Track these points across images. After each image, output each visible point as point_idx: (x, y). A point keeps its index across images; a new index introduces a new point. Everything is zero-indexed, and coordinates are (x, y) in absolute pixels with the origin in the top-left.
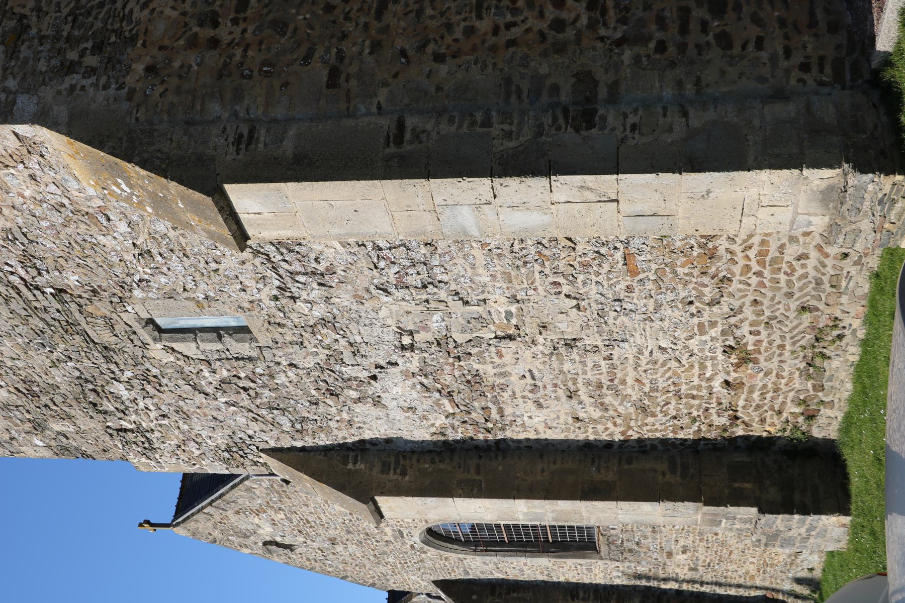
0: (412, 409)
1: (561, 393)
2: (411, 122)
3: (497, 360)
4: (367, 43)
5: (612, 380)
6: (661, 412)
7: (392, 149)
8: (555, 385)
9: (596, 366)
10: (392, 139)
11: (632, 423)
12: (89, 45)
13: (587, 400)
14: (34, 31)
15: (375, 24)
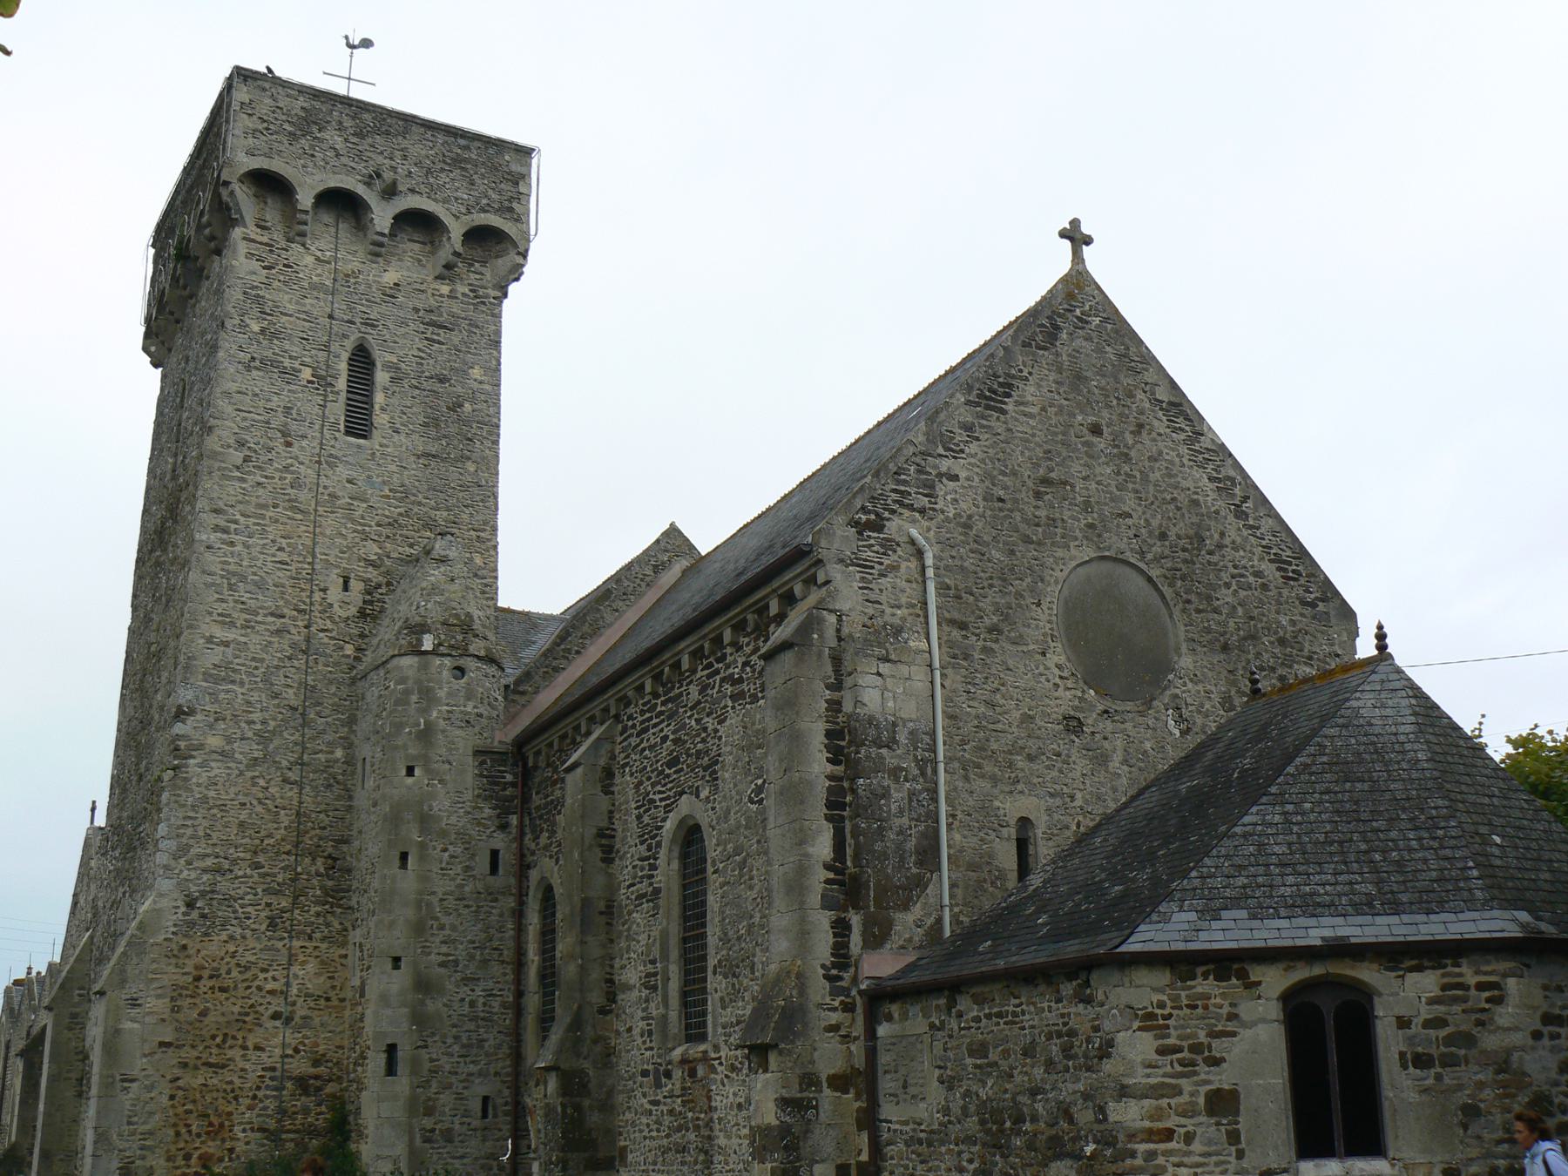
2: (135, 1085)
15: (199, 1063)
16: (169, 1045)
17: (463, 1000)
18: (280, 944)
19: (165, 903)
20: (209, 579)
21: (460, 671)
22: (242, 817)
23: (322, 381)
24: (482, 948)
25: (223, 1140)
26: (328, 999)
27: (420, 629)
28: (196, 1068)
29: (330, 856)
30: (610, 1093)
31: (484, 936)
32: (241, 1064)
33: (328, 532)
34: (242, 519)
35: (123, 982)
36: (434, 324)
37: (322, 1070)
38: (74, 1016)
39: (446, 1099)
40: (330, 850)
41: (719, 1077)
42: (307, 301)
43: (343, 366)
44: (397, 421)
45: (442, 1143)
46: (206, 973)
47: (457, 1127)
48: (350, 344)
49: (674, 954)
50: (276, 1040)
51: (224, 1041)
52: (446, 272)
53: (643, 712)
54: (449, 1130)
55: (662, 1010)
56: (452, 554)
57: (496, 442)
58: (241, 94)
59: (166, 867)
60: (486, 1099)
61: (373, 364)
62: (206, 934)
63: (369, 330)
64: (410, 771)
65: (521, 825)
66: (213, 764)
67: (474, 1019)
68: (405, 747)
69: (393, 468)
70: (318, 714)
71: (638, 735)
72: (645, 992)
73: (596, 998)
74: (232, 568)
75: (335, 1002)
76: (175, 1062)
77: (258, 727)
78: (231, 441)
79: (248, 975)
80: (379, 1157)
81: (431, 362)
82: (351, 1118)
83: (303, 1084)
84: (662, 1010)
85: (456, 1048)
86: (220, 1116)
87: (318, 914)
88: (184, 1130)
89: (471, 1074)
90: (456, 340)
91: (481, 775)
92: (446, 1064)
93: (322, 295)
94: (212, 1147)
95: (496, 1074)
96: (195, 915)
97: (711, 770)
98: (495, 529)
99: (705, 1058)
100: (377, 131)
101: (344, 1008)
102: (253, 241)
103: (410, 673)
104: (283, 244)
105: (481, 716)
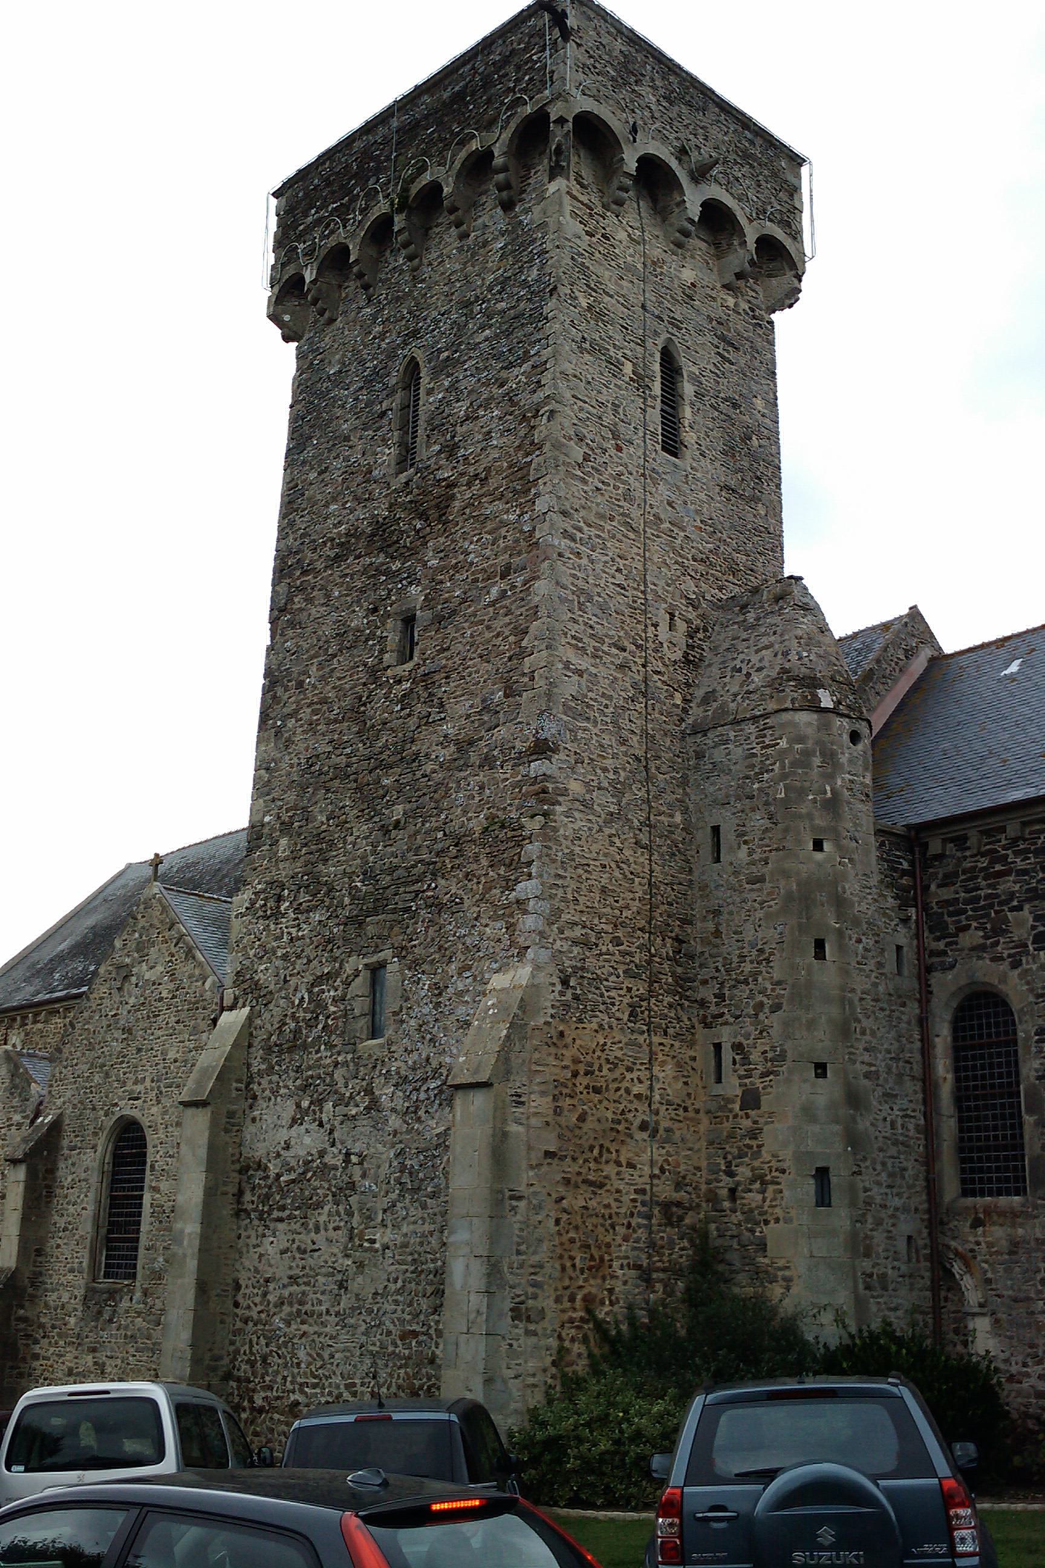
0: (287, 1147)
1: (297, 1272)
2: (522, 1204)
3: (331, 1226)
4: (569, 1176)
5: (306, 1313)
6: (271, 1351)
8: (304, 1268)
9: (320, 1302)
11: (260, 1327)
12: (579, 992)
13: (286, 1293)
14: (587, 953)
15: (580, 1179)
18: (641, 1039)
19: (542, 978)
20: (562, 592)
23: (640, 381)
24: (896, 1059)
25: (604, 1278)
31: (896, 1045)
34: (586, 528)
35: (508, 1072)
38: (231, 1115)
39: (879, 1237)
42: (624, 283)
43: (657, 367)
45: (879, 1292)
46: (582, 1068)
47: (890, 1272)
48: (660, 342)
50: (646, 1153)
51: (601, 1154)
57: (778, 486)
60: (910, 1238)
62: (580, 1021)
64: (818, 846)
66: (577, 815)
67: (896, 1143)
69: (702, 496)
70: (658, 768)
74: (580, 583)
76: (558, 1177)
79: (617, 1074)
86: (600, 1248)
87: (670, 1006)
91: (882, 858)
92: (876, 1192)
93: (636, 281)
94: (593, 1287)
103: (810, 731)
104: (599, 209)
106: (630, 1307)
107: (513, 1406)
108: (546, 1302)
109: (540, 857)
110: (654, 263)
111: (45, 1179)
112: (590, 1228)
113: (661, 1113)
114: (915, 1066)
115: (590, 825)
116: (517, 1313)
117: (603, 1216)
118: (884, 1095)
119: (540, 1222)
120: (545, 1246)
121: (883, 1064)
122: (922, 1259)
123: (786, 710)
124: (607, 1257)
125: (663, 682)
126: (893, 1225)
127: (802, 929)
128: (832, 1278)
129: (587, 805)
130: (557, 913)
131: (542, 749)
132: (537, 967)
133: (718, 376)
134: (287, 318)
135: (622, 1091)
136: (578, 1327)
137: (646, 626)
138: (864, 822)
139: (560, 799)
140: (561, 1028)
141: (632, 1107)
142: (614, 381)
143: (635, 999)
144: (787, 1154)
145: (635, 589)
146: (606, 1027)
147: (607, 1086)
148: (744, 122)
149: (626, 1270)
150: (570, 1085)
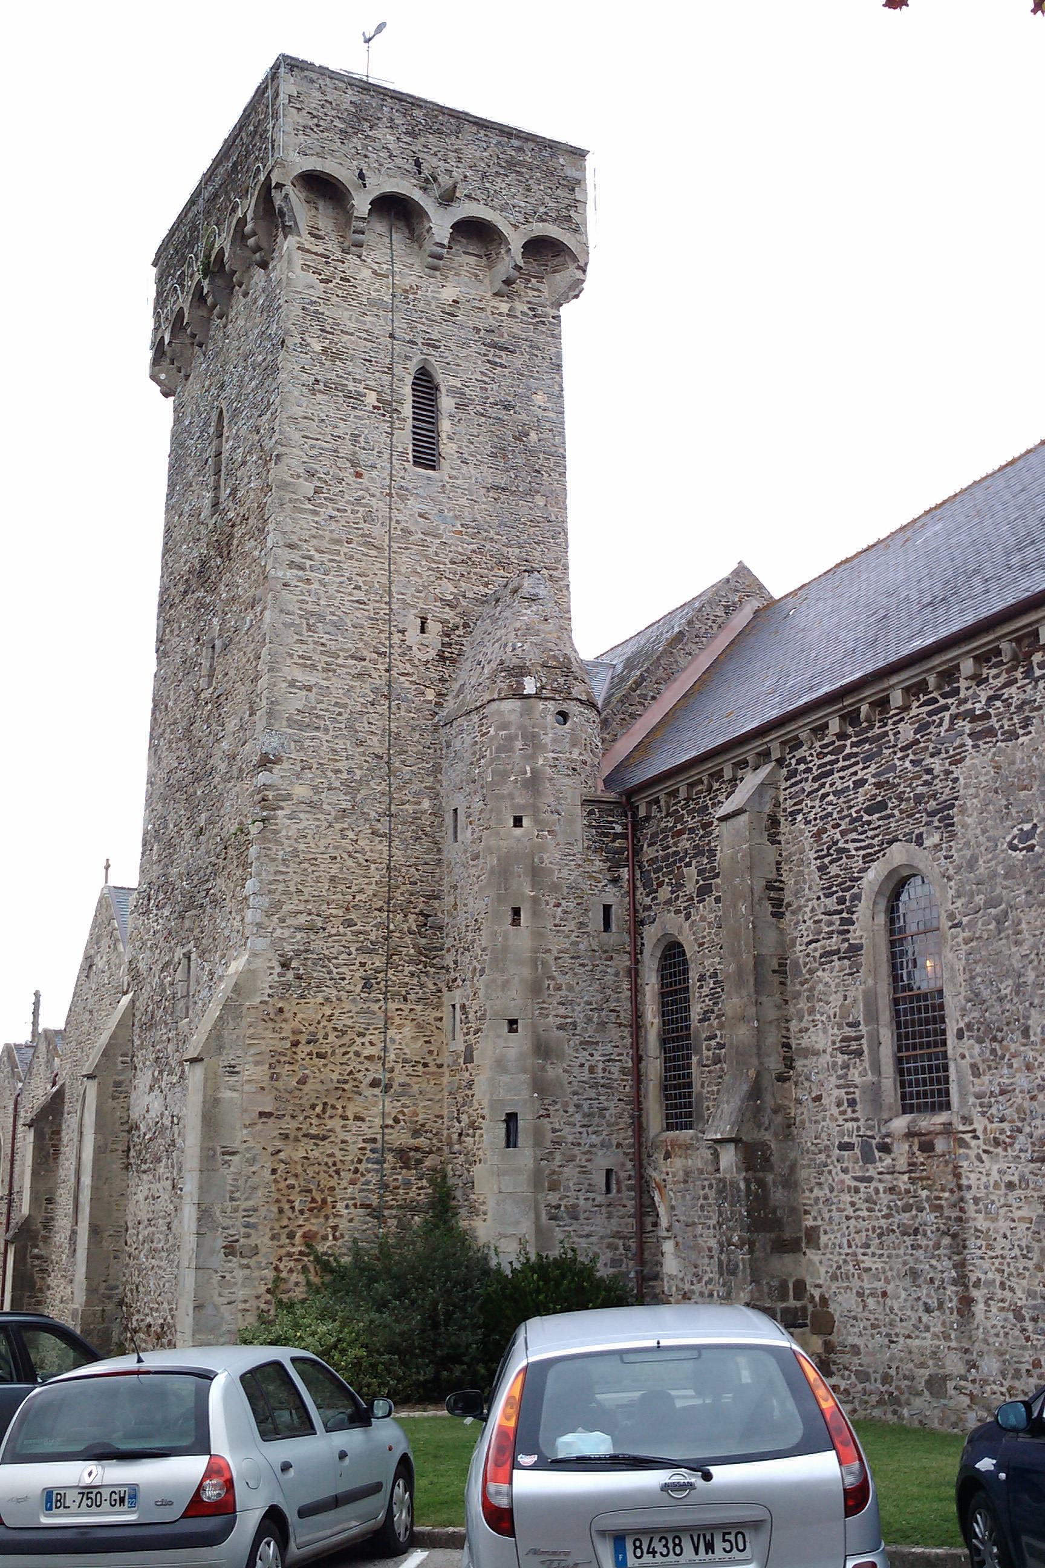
7: (219, 1150)
10: (884, 813)
14: (313, 937)
15: (300, 1134)
16: (269, 1115)
17: (582, 1065)
18: (375, 1007)
19: (260, 963)
20: (288, 619)
21: (564, 716)
22: (333, 872)
23: (387, 407)
25: (327, 1217)
26: (425, 1065)
27: (520, 672)
28: (297, 1140)
29: (421, 913)
30: (793, 1168)
32: (342, 1135)
33: (403, 570)
34: (317, 555)
35: (221, 1048)
36: (497, 346)
37: (421, 1141)
38: (118, 1084)
40: (421, 906)
41: (972, 1153)
42: (367, 319)
43: (408, 390)
44: (465, 450)
45: (568, 1221)
46: (303, 1039)
47: (582, 1202)
48: (413, 366)
49: (885, 1015)
50: (376, 1109)
51: (324, 1111)
52: (505, 288)
53: (821, 755)
54: (575, 1206)
55: (870, 1077)
56: (542, 592)
57: (563, 474)
58: (288, 86)
59: (259, 925)
60: (609, 1172)
61: (437, 389)
62: (302, 997)
63: (431, 351)
64: (518, 822)
65: (633, 880)
66: (302, 816)
67: (594, 1086)
68: (511, 796)
69: (463, 501)
70: (403, 762)
71: (814, 780)
72: (841, 1059)
73: (774, 1064)
74: (310, 607)
75: (432, 1068)
76: (275, 1133)
77: (345, 776)
78: (301, 471)
79: (346, 1039)
80: (502, 1236)
81: (495, 386)
82: (458, 1194)
83: (402, 1154)
84: (870, 1077)
85: (578, 1117)
86: (322, 1191)
88: (286, 1207)
89: (593, 1146)
90: (518, 363)
91: (590, 826)
94: (314, 1225)
95: (619, 1145)
96: (290, 975)
97: (944, 815)
98: (566, 568)
99: (947, 1130)
100: (429, 130)
101: (442, 1075)
102: (308, 251)
103: (513, 718)
104: (339, 255)
105: (585, 763)
106: (355, 1241)
107: (225, 1328)
108: (262, 1239)
109: (258, 858)
110: (406, 291)
111: (51, 1139)
112: (311, 1175)
113: (396, 1071)
114: (622, 1014)
115: (317, 823)
116: (230, 1250)
117: (326, 1164)
118: (581, 1043)
119: (254, 1173)
120: (260, 1193)
121: (582, 1015)
122: (624, 1188)
123: (494, 700)
124: (329, 1199)
125: (411, 682)
126: (588, 1160)
127: (500, 899)
128: (516, 1211)
129: (313, 806)
130: (278, 905)
131: (266, 762)
132: (254, 955)
133: (486, 383)
134: (163, 376)
135: (351, 1054)
136: (296, 1260)
137: (391, 634)
138: (569, 795)
139: (282, 804)
140: (280, 1005)
141: (362, 1067)
142: (353, 413)
143: (369, 972)
144: (485, 1103)
145: (377, 602)
146: (334, 999)
147: (334, 1051)
148: (507, 132)
149: (352, 1210)
150: (289, 1053)
